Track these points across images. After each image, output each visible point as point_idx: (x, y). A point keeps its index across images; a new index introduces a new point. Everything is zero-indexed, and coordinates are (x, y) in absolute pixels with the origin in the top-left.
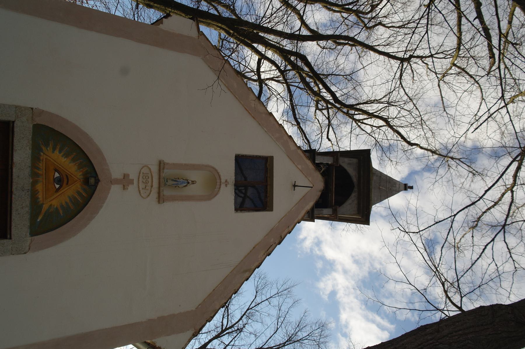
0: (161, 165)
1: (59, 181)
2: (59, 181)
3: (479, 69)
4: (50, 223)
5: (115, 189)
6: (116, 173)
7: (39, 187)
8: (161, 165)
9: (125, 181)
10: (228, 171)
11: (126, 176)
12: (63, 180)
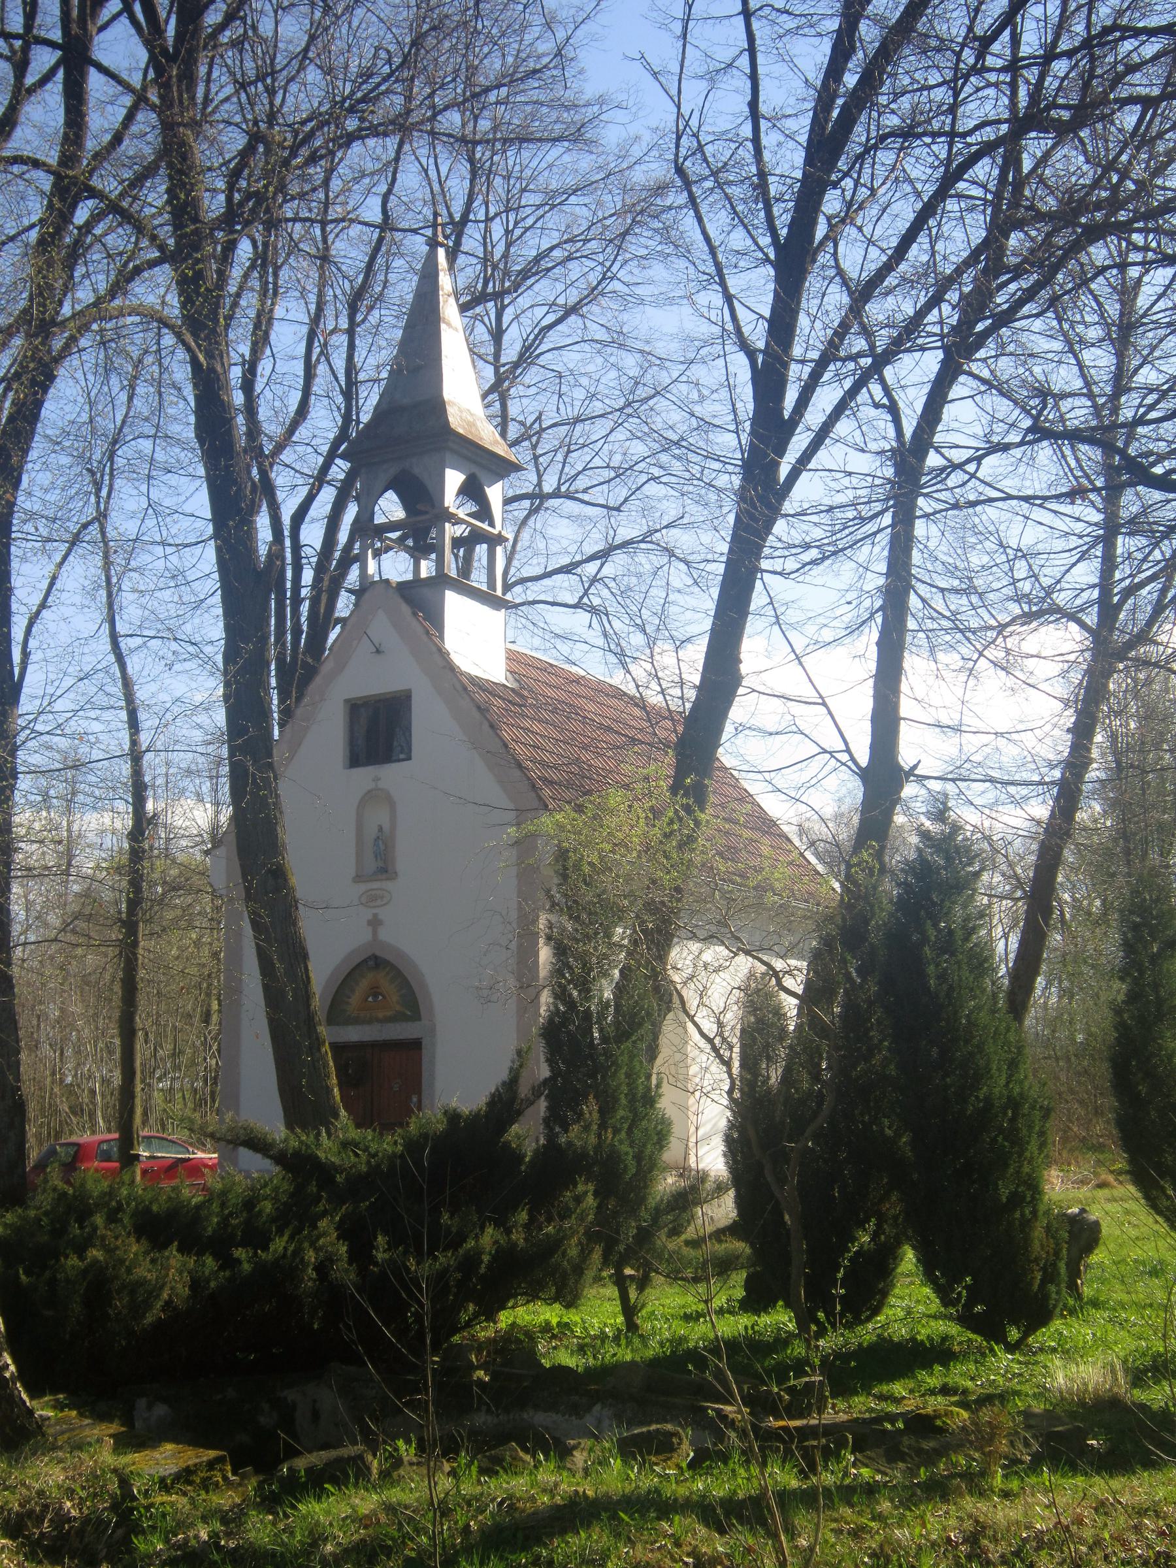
0: (359, 878)
1: (375, 995)
2: (375, 995)
3: (429, 232)
4: (412, 1005)
5: (384, 935)
6: (365, 936)
7: (380, 1015)
8: (359, 878)
9: (375, 923)
10: (364, 776)
11: (370, 923)
12: (375, 991)
